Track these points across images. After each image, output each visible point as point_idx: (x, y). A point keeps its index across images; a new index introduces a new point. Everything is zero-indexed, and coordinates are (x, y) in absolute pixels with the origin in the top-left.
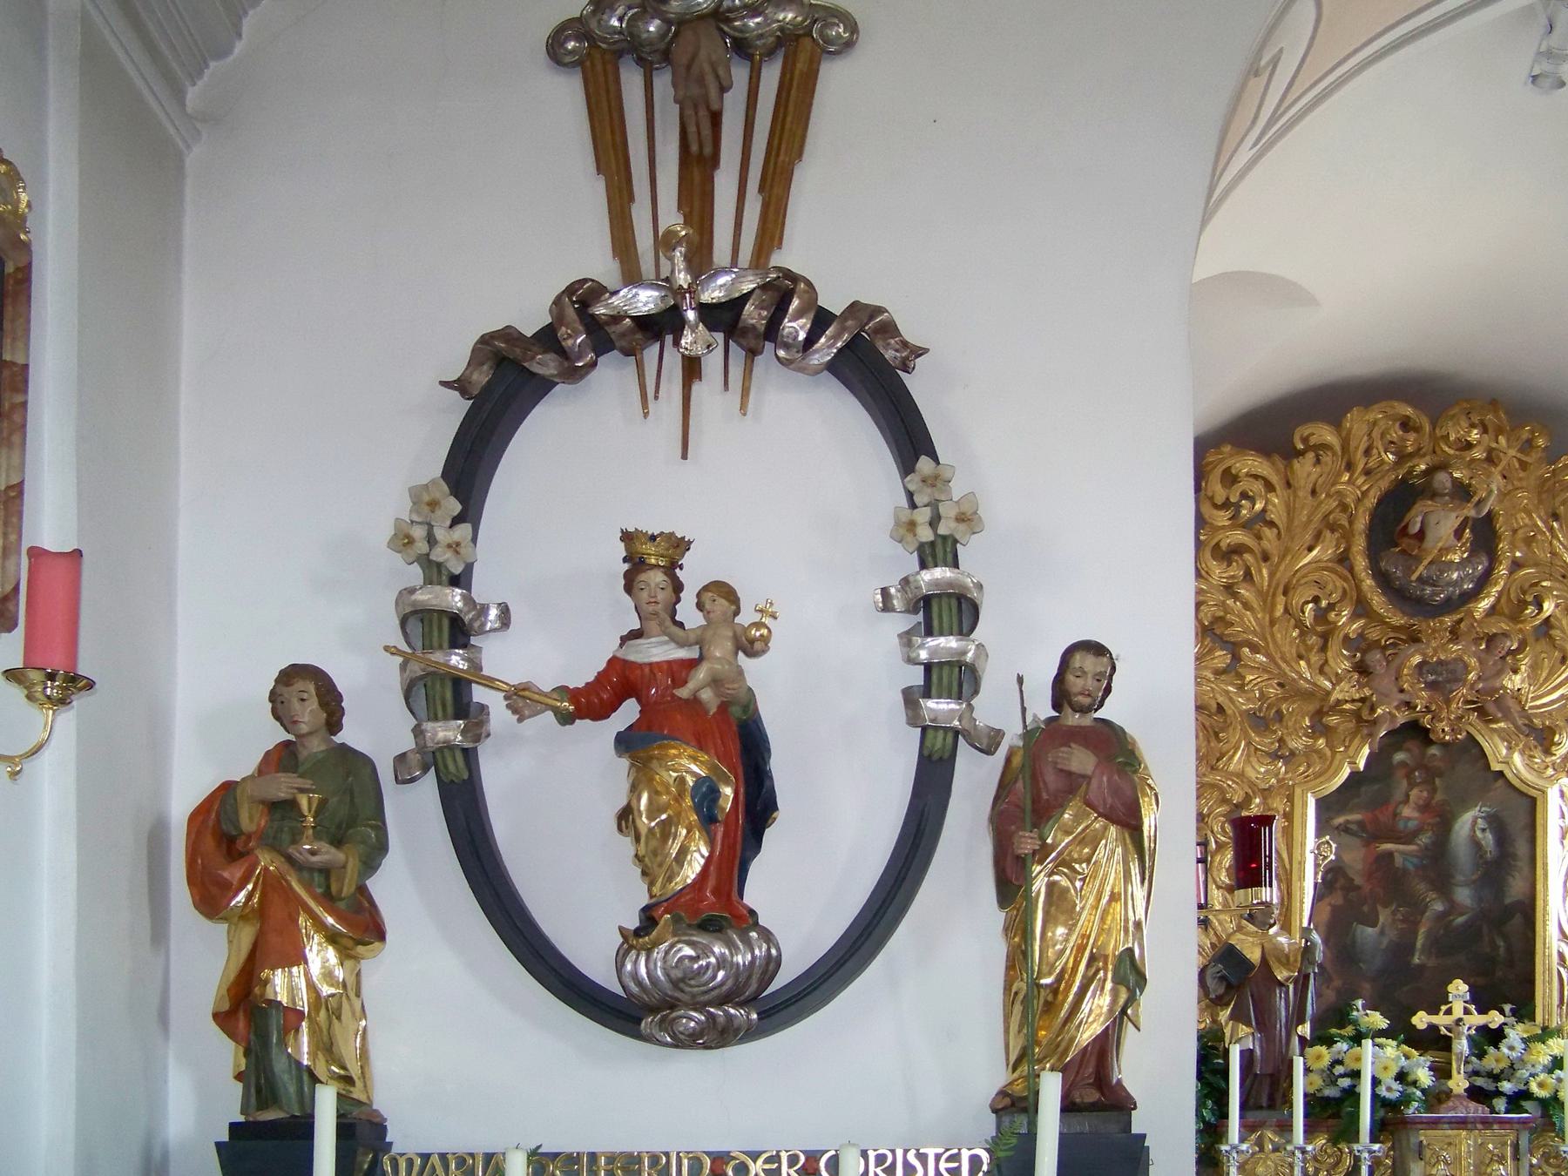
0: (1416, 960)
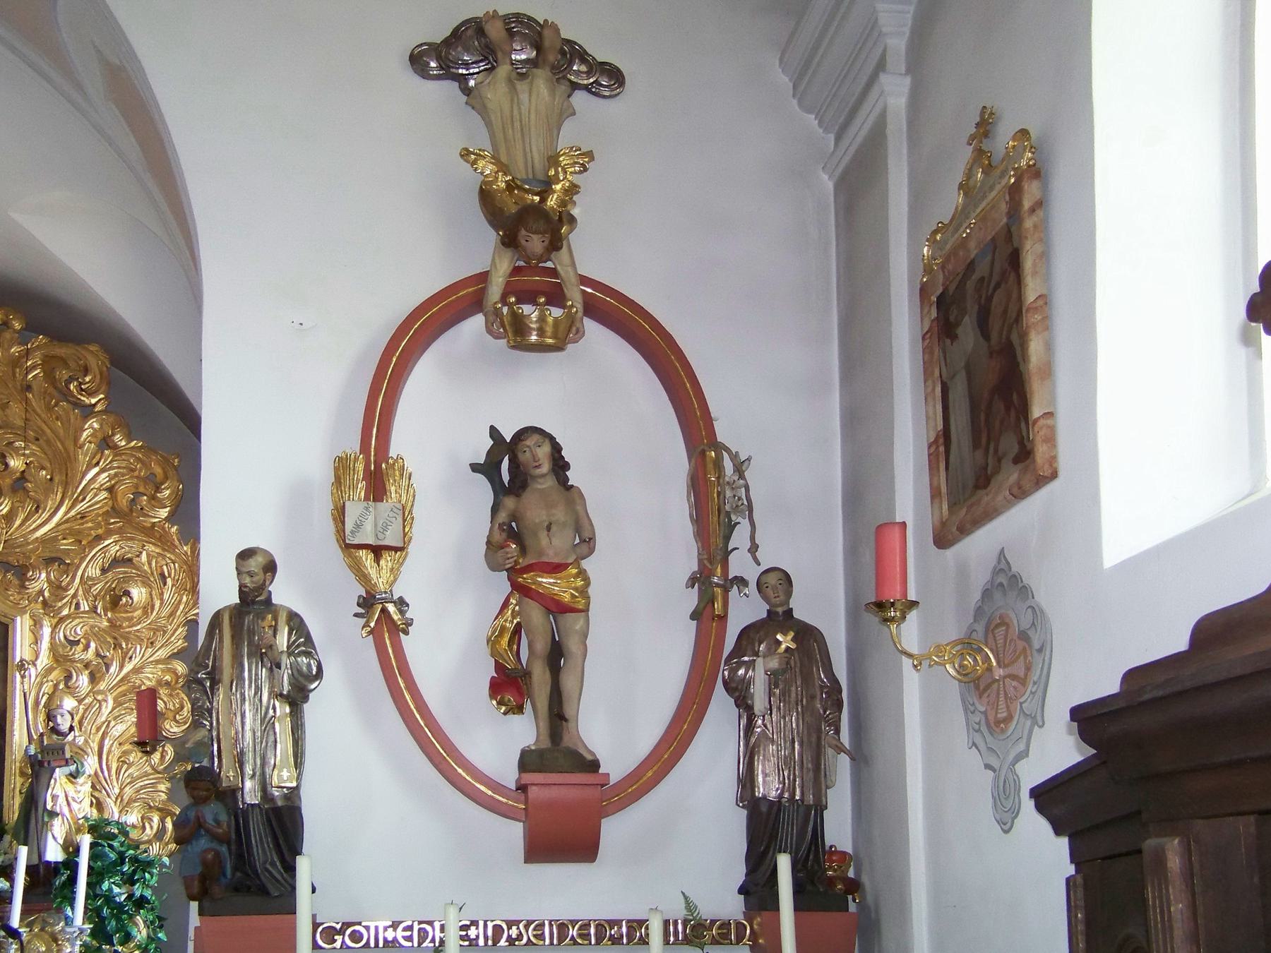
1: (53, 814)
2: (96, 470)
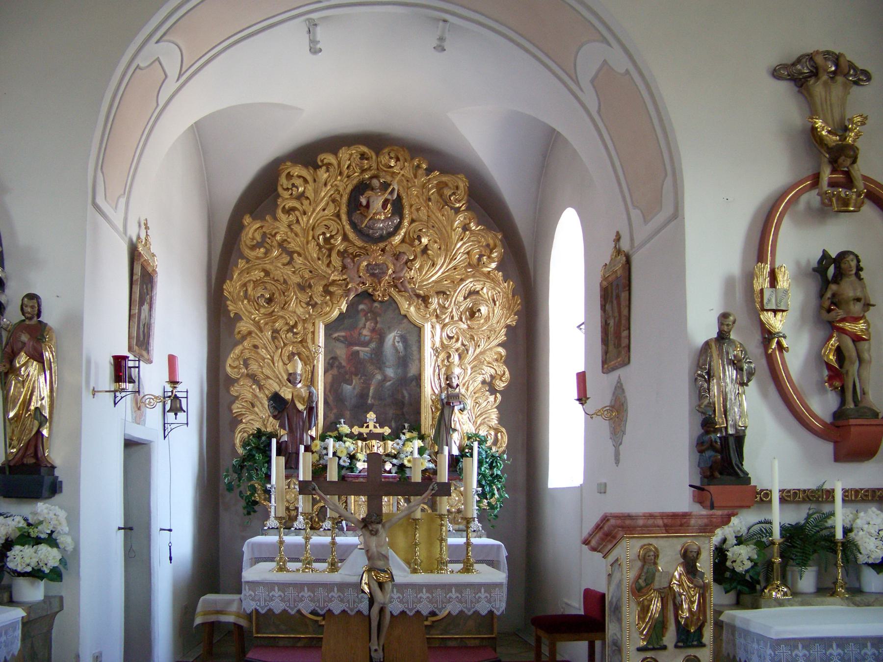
1: (455, 430)
2: (462, 242)
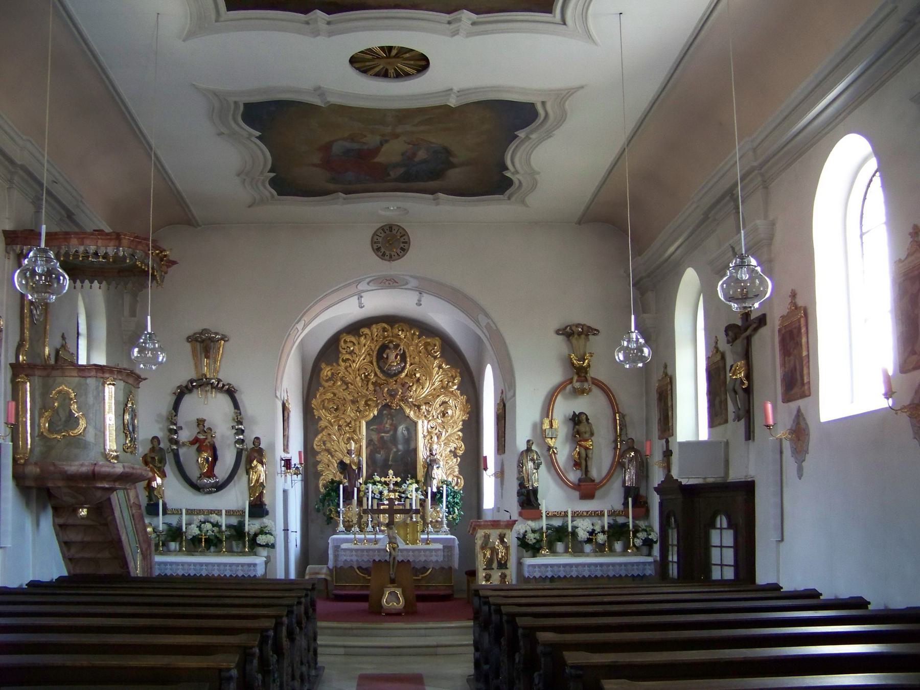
0: (390, 463)
1: (434, 478)
